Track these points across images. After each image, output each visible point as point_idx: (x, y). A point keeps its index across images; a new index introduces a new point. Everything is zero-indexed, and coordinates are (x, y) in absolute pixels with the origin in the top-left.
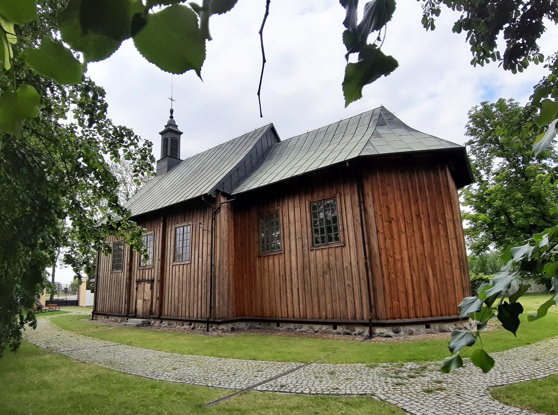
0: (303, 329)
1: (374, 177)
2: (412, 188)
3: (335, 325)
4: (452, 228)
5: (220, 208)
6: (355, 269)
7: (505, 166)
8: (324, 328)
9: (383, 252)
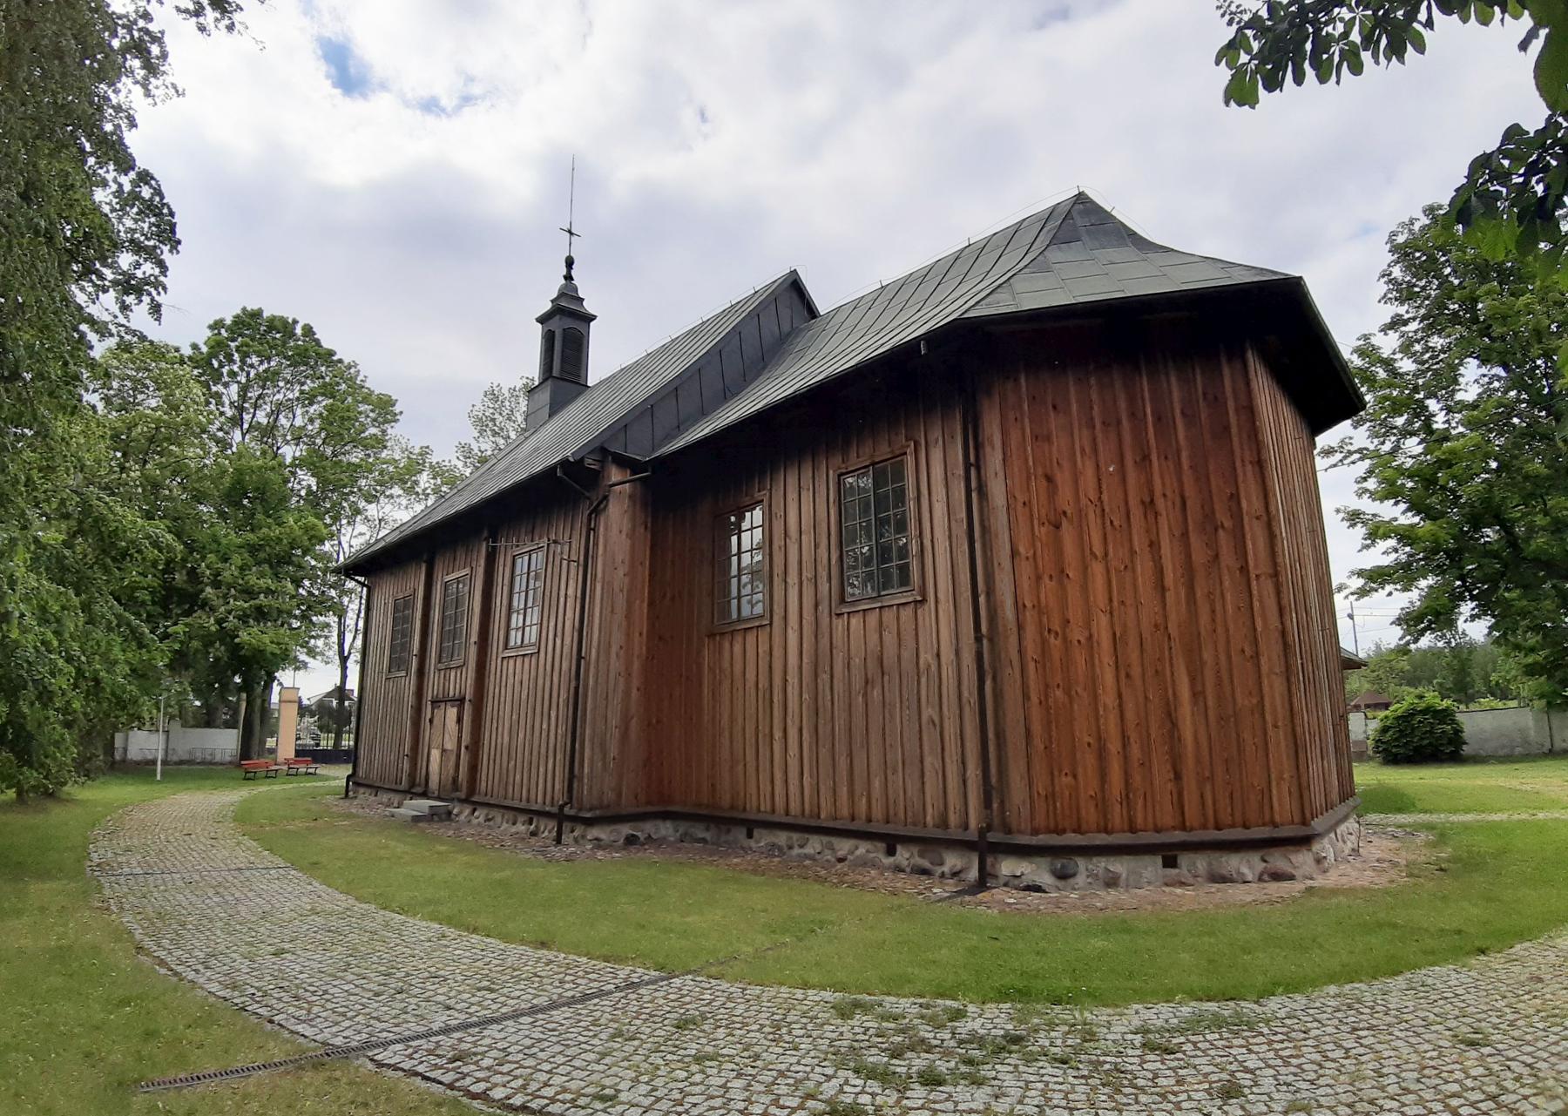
0: (809, 850)
1: (1010, 385)
2: (1132, 415)
3: (891, 843)
4: (1262, 542)
5: (606, 498)
6: (948, 672)
7: (1496, 384)
8: (863, 848)
9: (1030, 617)
